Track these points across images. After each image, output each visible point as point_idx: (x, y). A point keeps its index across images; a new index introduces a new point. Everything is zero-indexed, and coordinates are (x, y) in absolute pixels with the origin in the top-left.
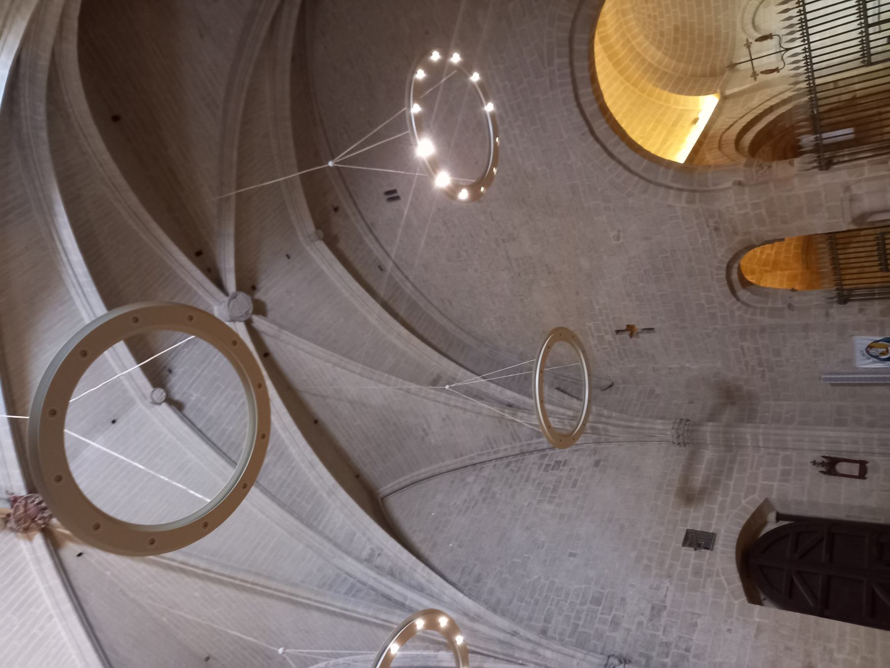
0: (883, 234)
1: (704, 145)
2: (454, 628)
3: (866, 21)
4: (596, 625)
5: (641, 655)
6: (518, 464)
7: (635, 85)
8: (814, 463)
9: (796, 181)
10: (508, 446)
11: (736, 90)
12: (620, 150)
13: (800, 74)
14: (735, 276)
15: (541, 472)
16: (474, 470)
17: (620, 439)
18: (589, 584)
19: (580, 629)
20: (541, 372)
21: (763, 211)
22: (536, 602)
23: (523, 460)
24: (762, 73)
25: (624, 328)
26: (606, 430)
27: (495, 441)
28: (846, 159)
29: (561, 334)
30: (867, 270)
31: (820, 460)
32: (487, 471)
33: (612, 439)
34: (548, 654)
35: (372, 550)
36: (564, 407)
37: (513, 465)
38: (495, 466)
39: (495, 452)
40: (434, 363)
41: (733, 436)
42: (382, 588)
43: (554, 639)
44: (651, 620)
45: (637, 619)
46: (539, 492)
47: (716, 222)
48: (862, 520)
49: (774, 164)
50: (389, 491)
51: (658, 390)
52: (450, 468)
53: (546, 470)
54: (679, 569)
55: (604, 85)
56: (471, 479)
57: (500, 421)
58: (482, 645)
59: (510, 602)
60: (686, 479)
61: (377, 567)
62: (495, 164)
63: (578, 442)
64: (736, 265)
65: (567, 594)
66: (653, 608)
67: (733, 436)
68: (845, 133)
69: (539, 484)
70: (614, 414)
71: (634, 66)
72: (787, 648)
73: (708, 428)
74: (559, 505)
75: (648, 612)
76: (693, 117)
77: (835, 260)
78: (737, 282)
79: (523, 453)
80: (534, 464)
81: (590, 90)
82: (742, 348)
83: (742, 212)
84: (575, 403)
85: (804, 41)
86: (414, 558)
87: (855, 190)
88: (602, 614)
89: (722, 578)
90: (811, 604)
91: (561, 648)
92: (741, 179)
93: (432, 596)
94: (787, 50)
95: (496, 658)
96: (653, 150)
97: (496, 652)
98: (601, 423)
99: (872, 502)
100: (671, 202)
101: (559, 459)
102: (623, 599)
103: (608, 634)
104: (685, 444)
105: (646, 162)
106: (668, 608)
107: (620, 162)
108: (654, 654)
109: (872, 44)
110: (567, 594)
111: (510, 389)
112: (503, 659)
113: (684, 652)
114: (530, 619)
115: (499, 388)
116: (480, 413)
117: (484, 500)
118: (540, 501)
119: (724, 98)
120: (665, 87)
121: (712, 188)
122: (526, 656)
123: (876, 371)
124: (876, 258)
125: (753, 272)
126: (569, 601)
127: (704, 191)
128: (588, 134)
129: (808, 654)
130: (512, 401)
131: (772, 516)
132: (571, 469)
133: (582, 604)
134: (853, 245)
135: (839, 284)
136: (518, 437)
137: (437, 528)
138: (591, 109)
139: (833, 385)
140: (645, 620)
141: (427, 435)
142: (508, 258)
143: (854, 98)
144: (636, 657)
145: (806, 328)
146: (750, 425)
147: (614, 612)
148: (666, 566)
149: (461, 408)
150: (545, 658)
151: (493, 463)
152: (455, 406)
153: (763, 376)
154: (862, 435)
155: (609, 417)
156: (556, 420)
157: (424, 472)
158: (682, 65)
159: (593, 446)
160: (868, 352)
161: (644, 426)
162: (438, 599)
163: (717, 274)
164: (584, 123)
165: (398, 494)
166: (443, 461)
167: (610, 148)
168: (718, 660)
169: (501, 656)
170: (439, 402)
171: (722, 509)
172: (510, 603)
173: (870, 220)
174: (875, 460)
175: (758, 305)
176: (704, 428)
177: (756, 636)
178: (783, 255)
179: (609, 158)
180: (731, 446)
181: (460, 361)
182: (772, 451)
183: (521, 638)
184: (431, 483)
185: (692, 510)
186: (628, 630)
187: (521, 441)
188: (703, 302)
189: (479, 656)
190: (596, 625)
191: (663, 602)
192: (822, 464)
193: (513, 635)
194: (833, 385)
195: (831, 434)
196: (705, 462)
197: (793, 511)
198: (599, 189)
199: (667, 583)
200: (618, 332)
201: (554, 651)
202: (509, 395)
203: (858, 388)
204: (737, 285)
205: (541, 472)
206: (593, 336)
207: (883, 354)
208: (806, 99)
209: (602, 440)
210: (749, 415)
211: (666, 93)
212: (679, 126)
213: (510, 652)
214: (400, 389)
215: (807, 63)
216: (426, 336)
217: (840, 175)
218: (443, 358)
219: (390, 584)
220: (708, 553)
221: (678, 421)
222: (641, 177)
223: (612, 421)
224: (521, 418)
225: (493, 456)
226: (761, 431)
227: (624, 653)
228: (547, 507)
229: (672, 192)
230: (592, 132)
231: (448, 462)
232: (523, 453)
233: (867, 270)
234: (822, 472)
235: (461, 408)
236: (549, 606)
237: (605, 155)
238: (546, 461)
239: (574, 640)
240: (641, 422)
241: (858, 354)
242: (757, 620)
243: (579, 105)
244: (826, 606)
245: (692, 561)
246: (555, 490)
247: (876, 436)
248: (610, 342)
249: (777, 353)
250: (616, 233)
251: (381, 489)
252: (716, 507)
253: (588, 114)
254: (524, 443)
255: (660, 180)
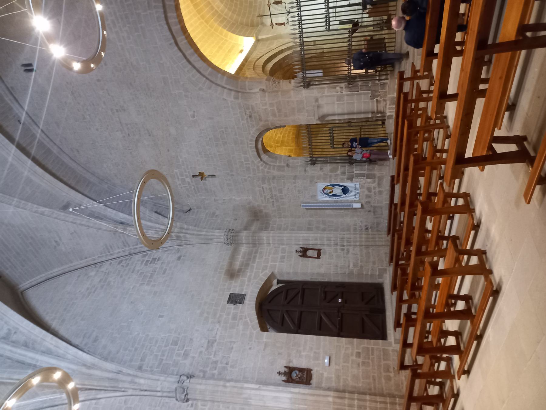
0: (333, 127)
1: (246, 66)
2: (66, 378)
3: (328, 5)
4: (174, 358)
5: (200, 371)
6: (128, 262)
7: (207, 22)
8: (296, 251)
9: (292, 93)
10: (120, 250)
11: (264, 37)
12: (194, 58)
13: (296, 29)
14: (260, 146)
15: (143, 265)
16: (95, 267)
17: (194, 242)
18: (171, 333)
19: (164, 362)
20: (138, 199)
21: (275, 108)
22: (136, 349)
23: (131, 259)
24: (276, 24)
25: (198, 174)
26: (185, 237)
27: (111, 247)
28: (317, 83)
29: (153, 174)
30: (325, 150)
31: (299, 249)
32: (105, 267)
33: (189, 243)
34: (142, 381)
35: (9, 330)
36: (159, 224)
37: (124, 262)
38: (111, 263)
39: (110, 255)
40: (64, 194)
41: (257, 238)
42: (17, 357)
43: (146, 371)
44: (207, 349)
45: (199, 350)
46: (141, 278)
47: (250, 112)
48: (317, 280)
49: (281, 81)
50: (28, 286)
51: (217, 213)
52: (76, 267)
53: (146, 264)
54: (225, 317)
55: (184, 12)
56: (93, 274)
57: (114, 234)
58: (96, 384)
59: (118, 352)
60: (231, 264)
61: (13, 342)
62: (103, 49)
63: (163, 246)
64: (261, 139)
65: (157, 341)
66: (209, 342)
67: (257, 238)
68: (318, 73)
69: (141, 273)
70: (190, 227)
71: (206, 10)
72: (280, 354)
73: (244, 234)
74: (154, 286)
75: (205, 346)
76: (240, 49)
77: (310, 144)
78: (262, 150)
79: (131, 254)
80: (138, 261)
81: (175, 14)
82: (263, 188)
83: (264, 108)
84: (166, 220)
85: (298, 9)
86: (44, 332)
87: (320, 102)
88: (178, 350)
89: (248, 319)
90: (293, 328)
91: (151, 376)
92: (264, 88)
93: (59, 356)
94: (289, 13)
95: (105, 390)
96: (217, 64)
97: (105, 387)
98: (182, 233)
99: (322, 270)
100: (225, 97)
101: (155, 257)
102: (191, 339)
103: (181, 362)
104: (231, 244)
105: (210, 69)
106: (217, 341)
107: (194, 67)
108: (208, 369)
109: (335, 138)
110: (157, 341)
111: (122, 212)
112: (111, 390)
113: (225, 365)
114: (131, 361)
115: (114, 212)
116: (100, 229)
117: (102, 287)
118: (141, 284)
119: (258, 41)
120: (225, 27)
121: (248, 91)
122: (126, 385)
123: (327, 202)
124: (329, 141)
125: (271, 147)
126: (157, 345)
127: (244, 93)
128: (174, 44)
129: (289, 355)
130: (123, 220)
131: (275, 282)
132: (162, 263)
133: (166, 346)
134: (320, 135)
135: (311, 154)
136: (127, 243)
137: (65, 309)
138: (176, 28)
139: (307, 209)
140: (203, 350)
141: (59, 245)
142: (121, 123)
143: (323, 52)
144: (197, 373)
145: (295, 177)
146: (266, 232)
147: (185, 348)
148: (218, 316)
149: (85, 226)
150: (140, 384)
151: (110, 262)
152: (81, 224)
153: (273, 205)
154: (319, 235)
155: (187, 229)
156: (153, 232)
157: (57, 270)
158: (235, 16)
159: (177, 247)
160: (323, 192)
161: (208, 234)
162: (63, 358)
163: (250, 144)
164: (170, 36)
165: (35, 288)
166: (72, 262)
167: (188, 57)
168: (244, 366)
169: (109, 389)
170: (68, 222)
171: (249, 280)
172: (117, 353)
173: (327, 119)
174: (326, 249)
175: (272, 164)
176: (241, 234)
177: (264, 350)
178: (286, 138)
179: (187, 63)
180: (255, 244)
181: (86, 193)
182: (277, 245)
183: (124, 374)
184: (62, 278)
185: (233, 282)
186: (193, 357)
187: (129, 246)
188: (243, 160)
189: (94, 391)
190: (174, 358)
191: (215, 337)
192: (300, 252)
193: (118, 373)
194: (307, 209)
195: (305, 235)
196: (241, 254)
197: (285, 278)
198: (182, 83)
199: (217, 326)
200: (194, 176)
201: (145, 378)
202: (122, 216)
203: (318, 211)
204: (261, 152)
205: (143, 265)
206: (178, 178)
207: (330, 192)
208: (299, 49)
209: (183, 244)
210: (265, 227)
211: (225, 31)
212: (232, 52)
213: (116, 385)
214: (35, 212)
215: (297, 5)
216: (58, 174)
217: (314, 92)
218: (72, 190)
219: (23, 352)
220: (240, 306)
221: (228, 230)
222: (207, 78)
223: (189, 232)
224: (130, 231)
225: (110, 257)
226: (271, 235)
227: (190, 373)
228: (146, 288)
229: (226, 90)
230: (177, 44)
231: (75, 263)
232: (131, 254)
233: (325, 150)
234: (300, 256)
235: (85, 226)
236: (144, 351)
237: (185, 60)
238: (146, 259)
239: (160, 370)
240: (207, 231)
241: (319, 193)
242: (265, 340)
243: (168, 23)
244: (299, 328)
245: (232, 311)
246: (151, 277)
247: (325, 236)
248: (189, 183)
249: (280, 191)
250: (192, 113)
251: (21, 286)
252: (246, 279)
253: (174, 31)
254: (131, 247)
255: (219, 82)
